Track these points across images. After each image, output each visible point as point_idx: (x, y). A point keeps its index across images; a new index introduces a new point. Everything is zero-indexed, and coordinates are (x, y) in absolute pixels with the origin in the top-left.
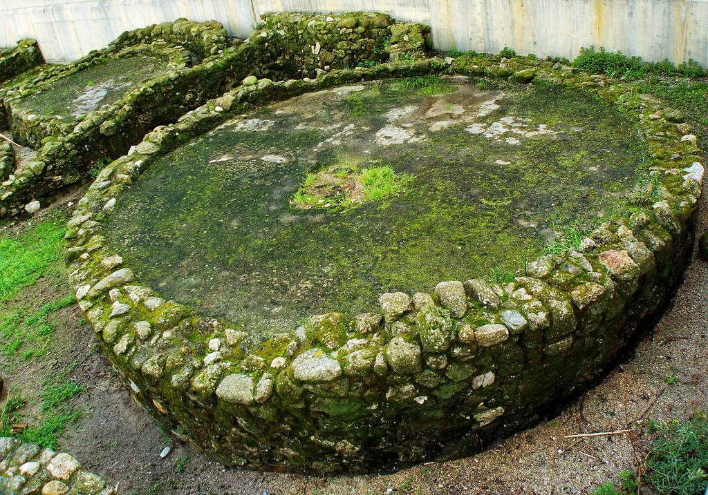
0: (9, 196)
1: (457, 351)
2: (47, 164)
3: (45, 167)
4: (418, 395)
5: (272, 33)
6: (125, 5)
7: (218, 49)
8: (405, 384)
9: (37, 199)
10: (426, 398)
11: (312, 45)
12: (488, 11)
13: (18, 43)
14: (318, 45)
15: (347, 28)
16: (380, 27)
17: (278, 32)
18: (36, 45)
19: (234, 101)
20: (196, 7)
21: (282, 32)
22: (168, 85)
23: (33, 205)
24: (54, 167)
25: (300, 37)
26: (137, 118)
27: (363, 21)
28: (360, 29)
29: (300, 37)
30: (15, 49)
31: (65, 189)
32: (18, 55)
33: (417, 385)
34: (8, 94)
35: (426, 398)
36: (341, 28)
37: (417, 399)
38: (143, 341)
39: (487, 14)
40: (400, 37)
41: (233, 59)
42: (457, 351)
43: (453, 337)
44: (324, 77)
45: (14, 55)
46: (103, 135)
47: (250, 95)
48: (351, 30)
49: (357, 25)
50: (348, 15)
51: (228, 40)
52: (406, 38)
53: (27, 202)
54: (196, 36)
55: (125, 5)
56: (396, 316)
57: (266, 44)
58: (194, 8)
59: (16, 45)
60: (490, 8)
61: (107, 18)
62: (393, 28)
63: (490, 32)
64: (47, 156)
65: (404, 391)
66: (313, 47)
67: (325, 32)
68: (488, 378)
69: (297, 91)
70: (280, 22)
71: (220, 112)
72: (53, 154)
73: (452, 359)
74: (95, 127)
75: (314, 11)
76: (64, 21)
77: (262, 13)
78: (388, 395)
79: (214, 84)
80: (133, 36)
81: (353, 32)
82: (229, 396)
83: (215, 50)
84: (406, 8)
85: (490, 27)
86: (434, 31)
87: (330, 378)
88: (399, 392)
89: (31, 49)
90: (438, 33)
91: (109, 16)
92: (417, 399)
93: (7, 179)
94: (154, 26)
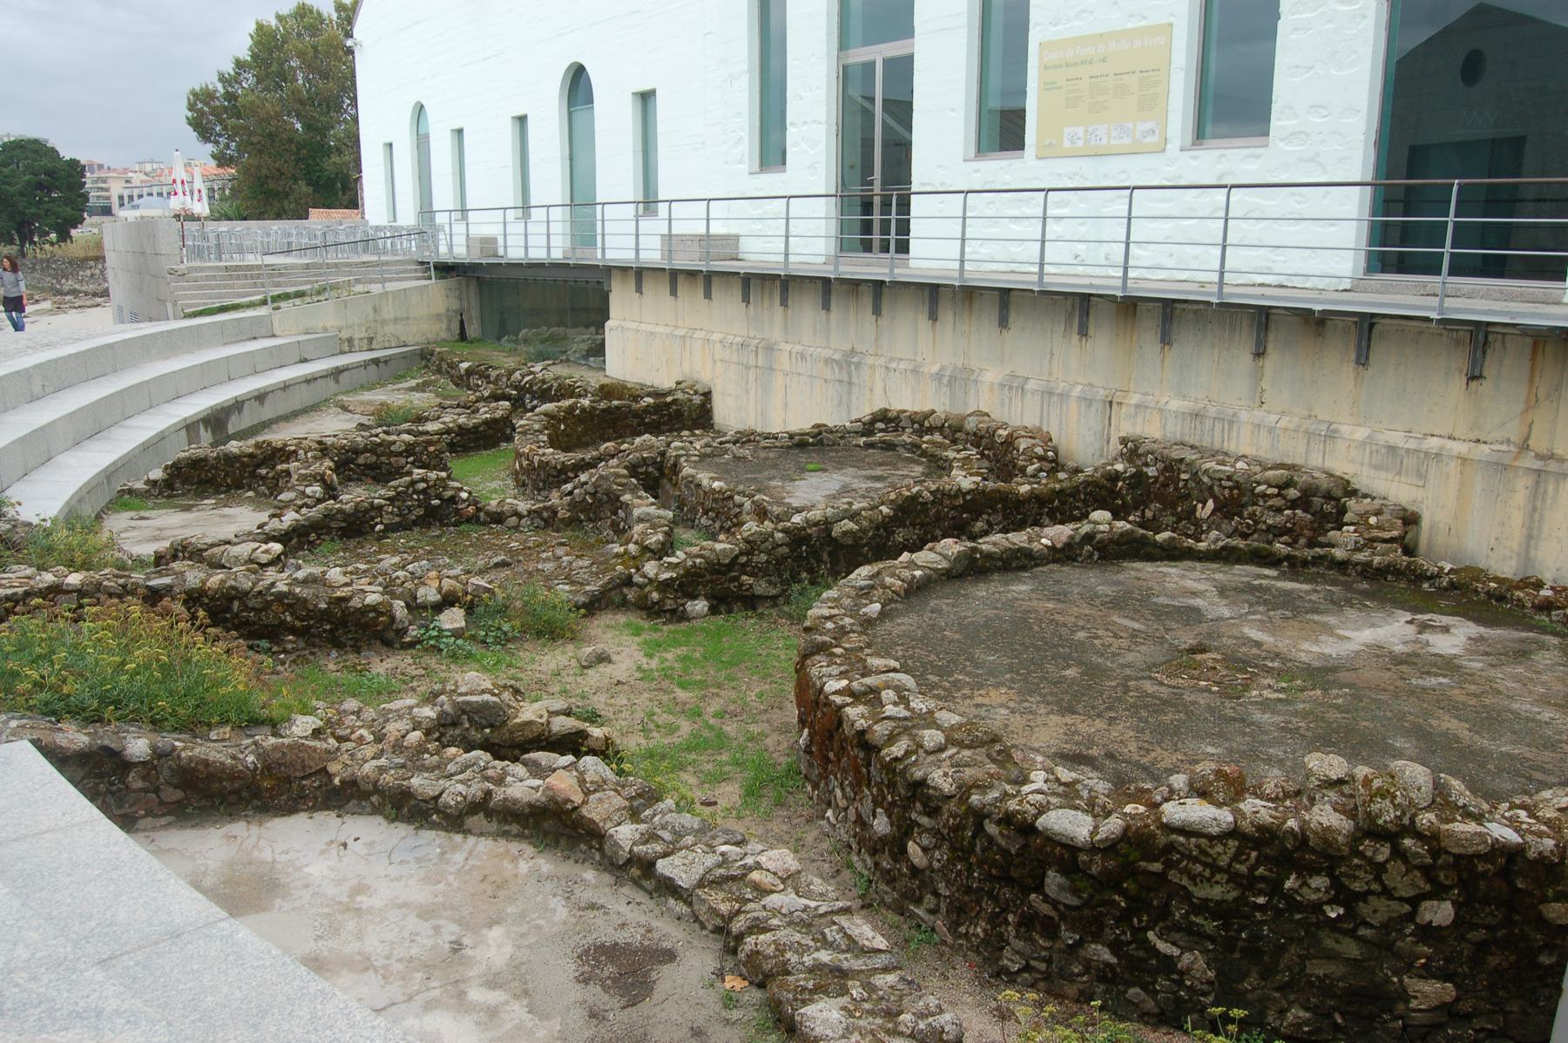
0: (671, 578)
1: (1408, 842)
2: (741, 553)
3: (737, 557)
4: (1329, 902)
5: (1134, 470)
6: (887, 368)
7: (1041, 470)
8: (1318, 873)
9: (707, 599)
10: (1341, 911)
11: (1198, 502)
12: (1538, 504)
13: (678, 383)
14: (1210, 504)
15: (1270, 486)
16: (1328, 496)
17: (1145, 469)
18: (707, 395)
19: (1072, 537)
20: (1010, 399)
21: (1151, 471)
22: (956, 496)
23: (700, 606)
24: (749, 561)
25: (1181, 484)
26: (894, 532)
27: (1302, 479)
28: (1293, 493)
29: (1181, 484)
30: (670, 392)
31: (751, 602)
32: (675, 401)
33: (1336, 883)
34: (672, 445)
35: (1341, 911)
36: (1259, 484)
37: (1327, 908)
38: (929, 753)
39: (1534, 509)
40: (1364, 516)
41: (1062, 491)
42: (1408, 842)
43: (1406, 821)
44: (1220, 544)
45: (669, 399)
46: (835, 540)
47: (1099, 536)
48: (1275, 491)
49: (1289, 484)
50: (1282, 466)
51: (1054, 464)
52: (1373, 520)
53: (694, 597)
54: (1002, 443)
55: (887, 368)
56: (1325, 782)
57: (1120, 484)
58: (1007, 401)
59: (674, 386)
60: (1544, 500)
61: (850, 383)
62: (1351, 503)
63: (1533, 543)
64: (746, 541)
65: (1313, 886)
66: (1200, 505)
67: (1230, 484)
68: (1440, 913)
69: (1172, 553)
70: (1152, 453)
71: (1046, 546)
72: (755, 542)
73: (1399, 853)
74: (827, 524)
75: (1217, 446)
76: (772, 369)
77: (1123, 434)
78: (1288, 884)
79: (1019, 513)
80: (896, 418)
81: (1278, 495)
82: (1056, 827)
83: (1035, 470)
84: (1383, 475)
85: (1535, 533)
86: (1425, 523)
87: (1214, 830)
88: (1305, 884)
89: (697, 400)
90: (1430, 538)
91: (855, 379)
92: (1327, 908)
93: (673, 554)
94: (933, 412)
